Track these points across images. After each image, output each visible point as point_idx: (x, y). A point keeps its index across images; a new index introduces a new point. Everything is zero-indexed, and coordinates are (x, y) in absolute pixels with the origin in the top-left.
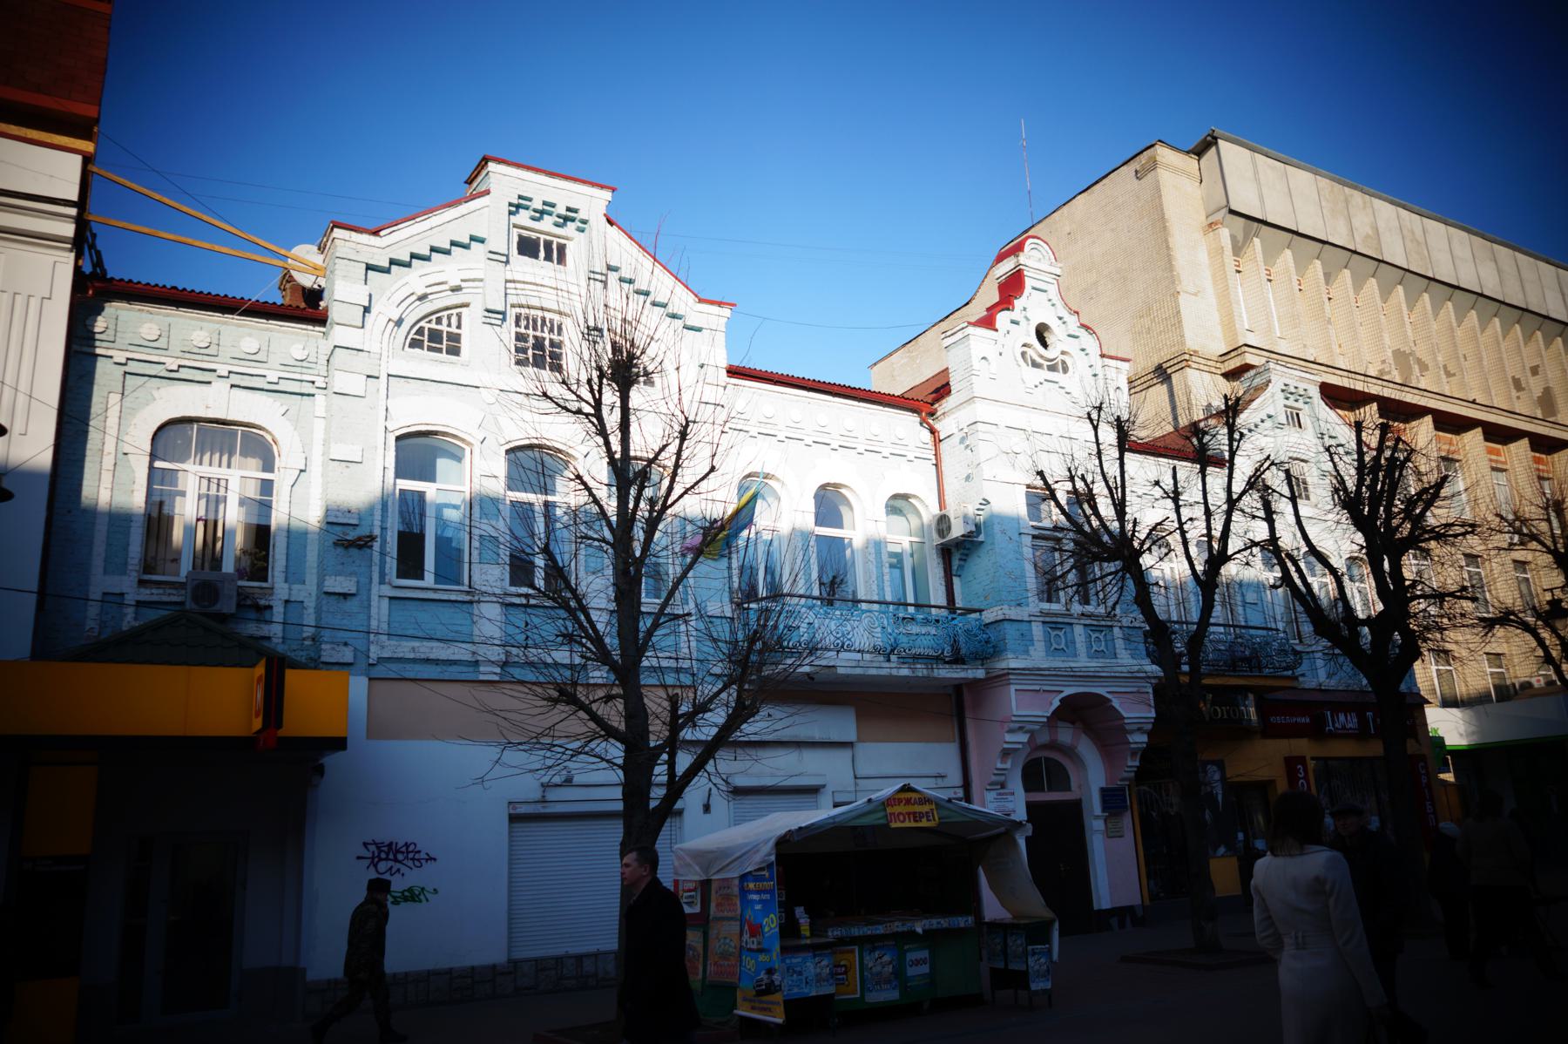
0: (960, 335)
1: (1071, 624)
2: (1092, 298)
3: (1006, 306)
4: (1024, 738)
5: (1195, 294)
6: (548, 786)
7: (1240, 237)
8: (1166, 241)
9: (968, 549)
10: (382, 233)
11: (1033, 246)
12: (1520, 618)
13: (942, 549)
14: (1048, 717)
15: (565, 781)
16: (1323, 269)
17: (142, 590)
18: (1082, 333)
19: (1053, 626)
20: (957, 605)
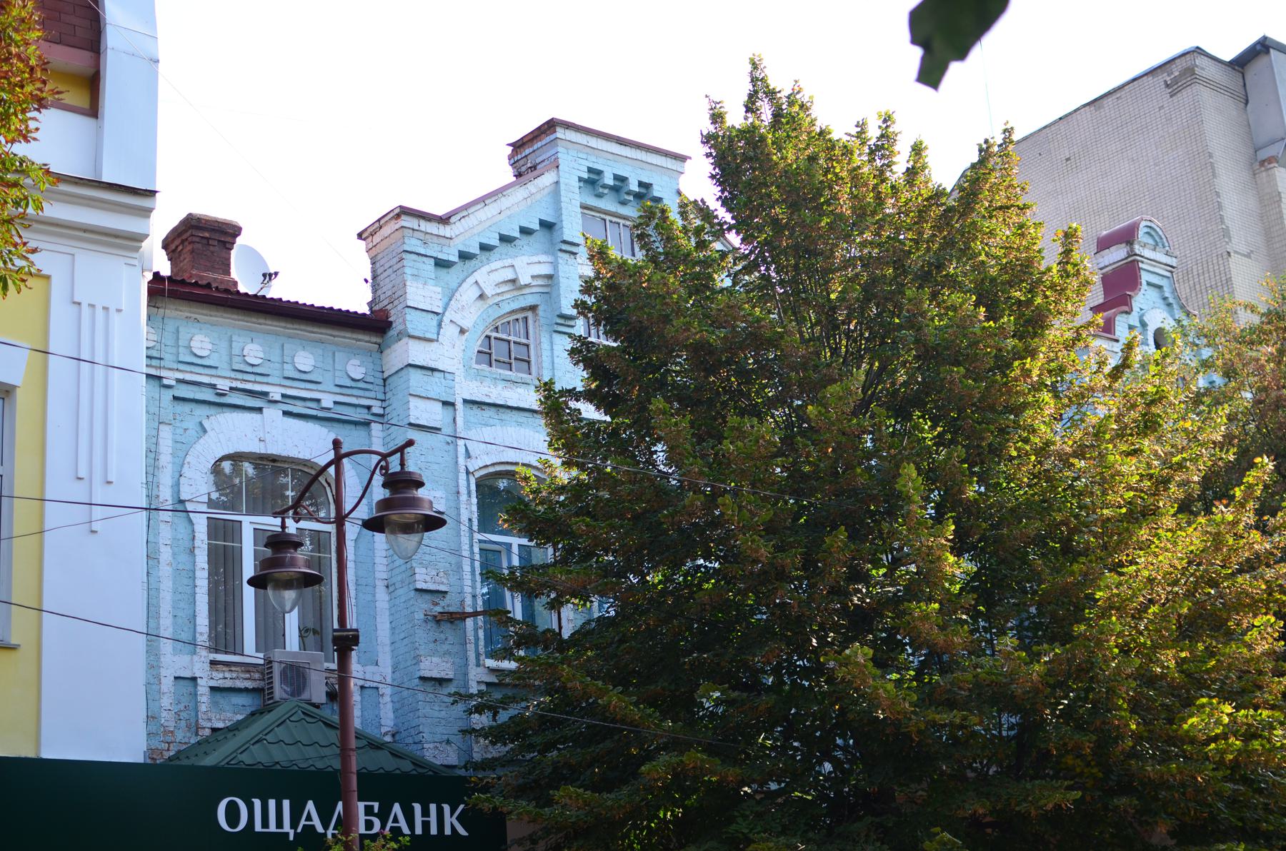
17: (215, 674)
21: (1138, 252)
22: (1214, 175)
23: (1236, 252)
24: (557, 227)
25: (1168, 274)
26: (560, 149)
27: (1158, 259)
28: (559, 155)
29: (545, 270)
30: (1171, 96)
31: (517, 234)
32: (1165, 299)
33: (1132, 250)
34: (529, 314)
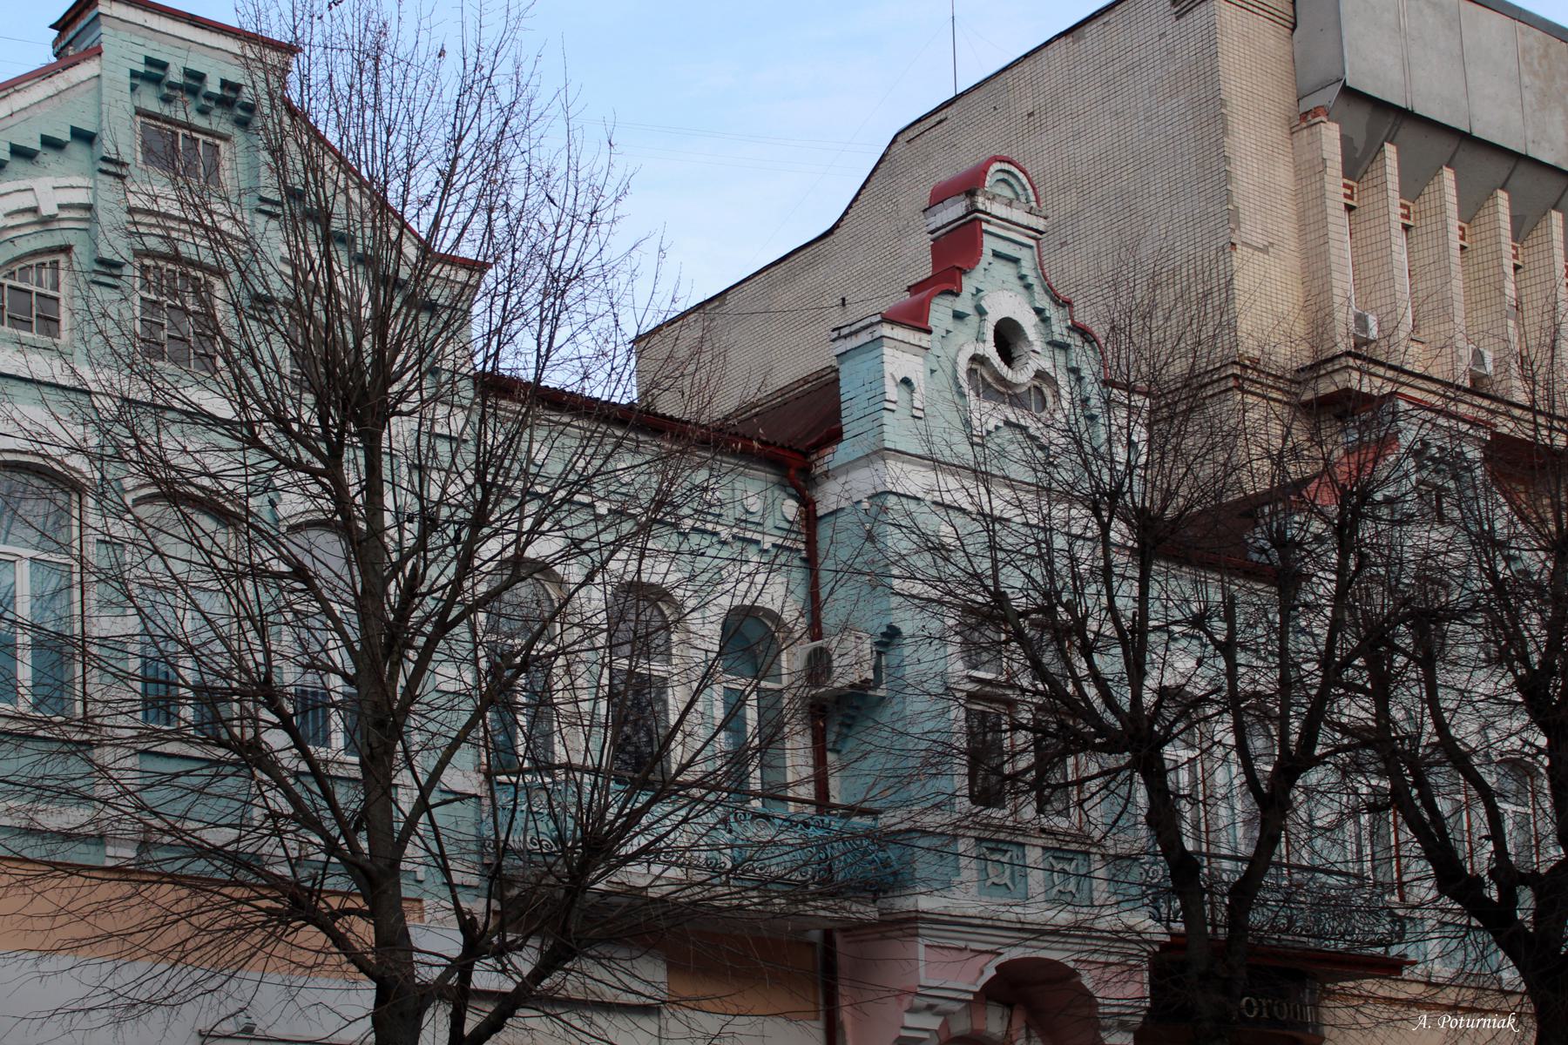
0: (864, 337)
1: (1022, 845)
2: (1063, 244)
3: (946, 286)
4: (934, 1023)
5: (1265, 250)
6: (209, 1036)
7: (1360, 141)
8: (1219, 145)
9: (857, 708)
10: (878, 318)
11: (1001, 176)
12: (289, 440)
13: (812, 706)
14: (974, 993)
15: (242, 1032)
16: (1511, 208)
18: (1075, 340)
19: (992, 845)
20: (832, 800)
21: (981, 207)
22: (1225, 131)
23: (1245, 244)
24: (97, 140)
25: (1032, 242)
26: (103, 29)
27: (1014, 219)
28: (103, 38)
29: (81, 197)
30: (1178, 18)
31: (37, 146)
32: (1022, 277)
33: (973, 203)
34: (62, 259)
